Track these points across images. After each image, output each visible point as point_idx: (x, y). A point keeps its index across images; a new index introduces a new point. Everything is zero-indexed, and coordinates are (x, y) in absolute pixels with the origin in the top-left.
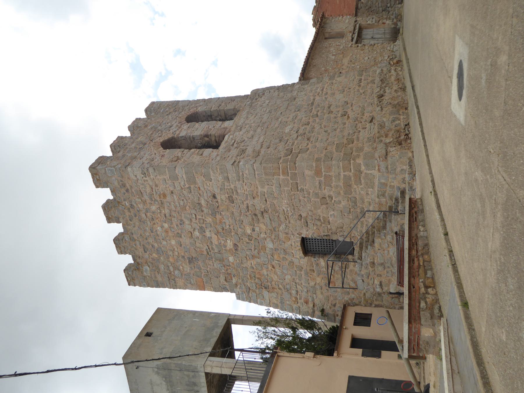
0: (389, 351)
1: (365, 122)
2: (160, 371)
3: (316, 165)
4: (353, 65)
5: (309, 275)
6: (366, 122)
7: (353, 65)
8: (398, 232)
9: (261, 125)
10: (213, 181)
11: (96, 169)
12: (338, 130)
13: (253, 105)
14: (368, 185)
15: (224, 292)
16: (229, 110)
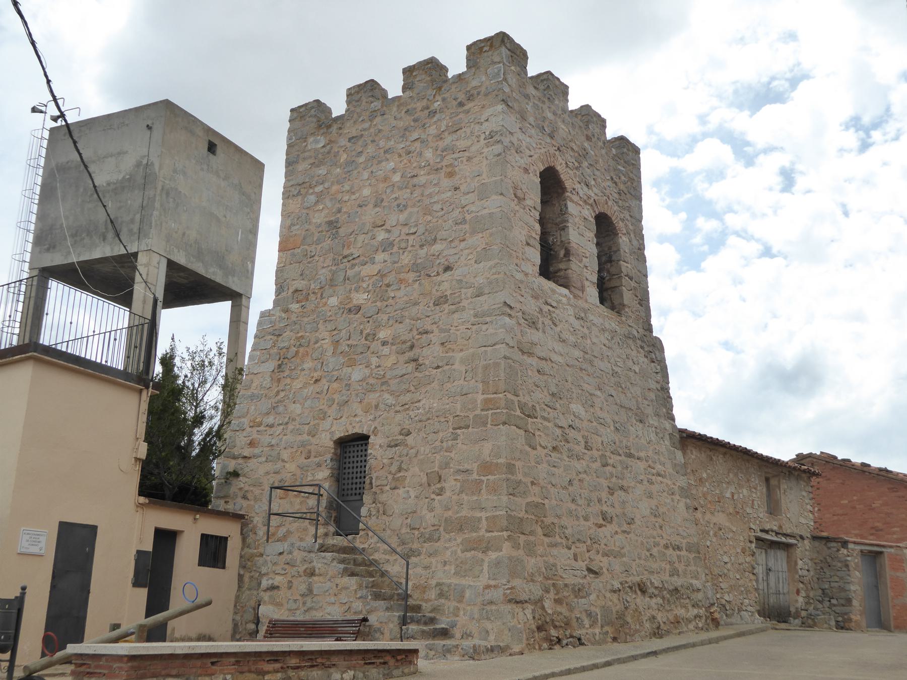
0: (170, 596)
1: (590, 558)
2: (141, 170)
3: (501, 463)
4: (711, 533)
5: (301, 449)
6: (588, 560)
7: (711, 533)
8: (367, 623)
9: (586, 356)
10: (476, 266)
11: (500, 46)
12: (573, 507)
13: (630, 342)
14: (461, 565)
15: (274, 287)
16: (622, 296)
